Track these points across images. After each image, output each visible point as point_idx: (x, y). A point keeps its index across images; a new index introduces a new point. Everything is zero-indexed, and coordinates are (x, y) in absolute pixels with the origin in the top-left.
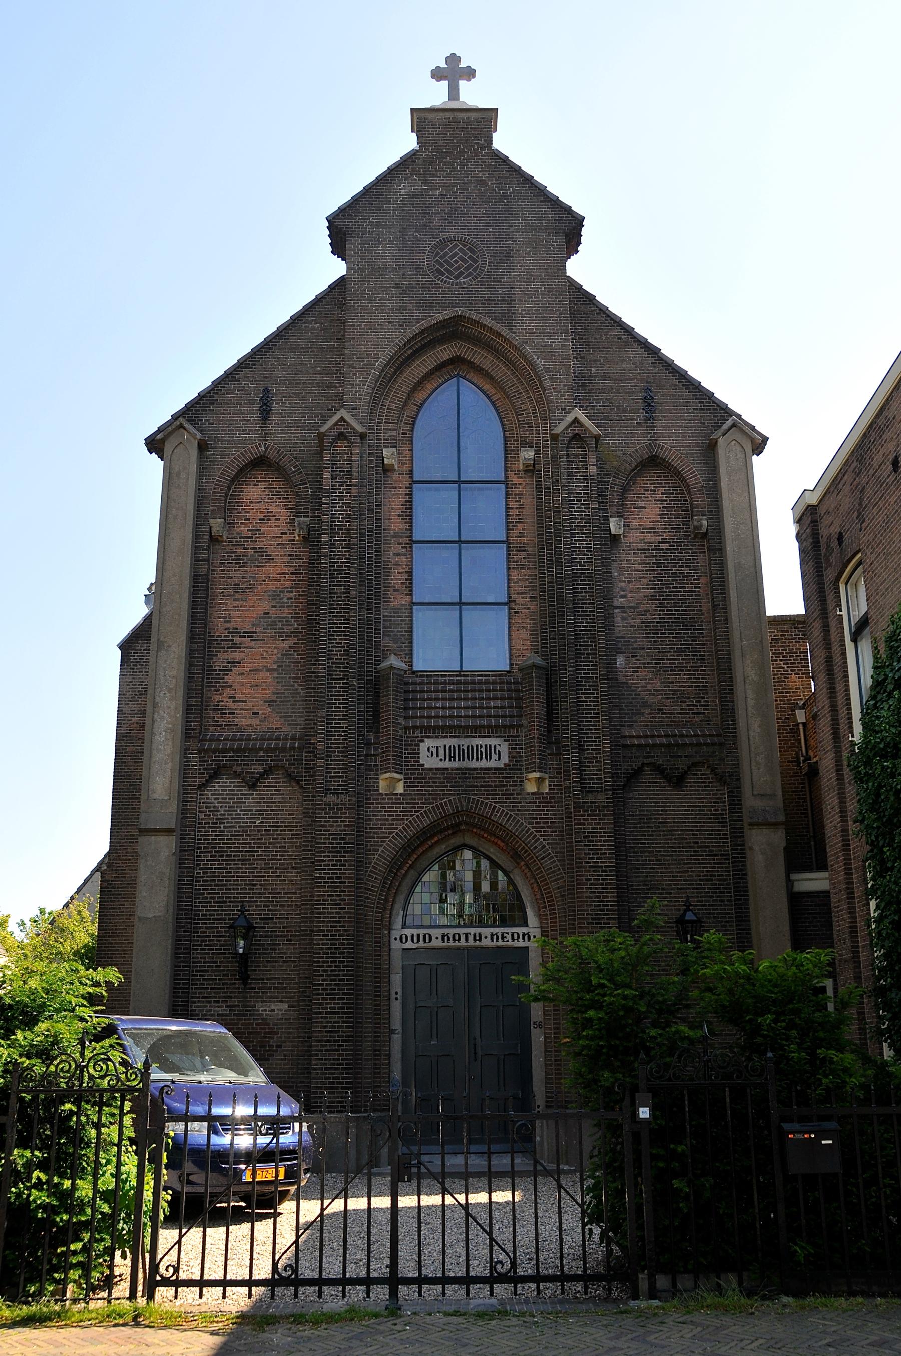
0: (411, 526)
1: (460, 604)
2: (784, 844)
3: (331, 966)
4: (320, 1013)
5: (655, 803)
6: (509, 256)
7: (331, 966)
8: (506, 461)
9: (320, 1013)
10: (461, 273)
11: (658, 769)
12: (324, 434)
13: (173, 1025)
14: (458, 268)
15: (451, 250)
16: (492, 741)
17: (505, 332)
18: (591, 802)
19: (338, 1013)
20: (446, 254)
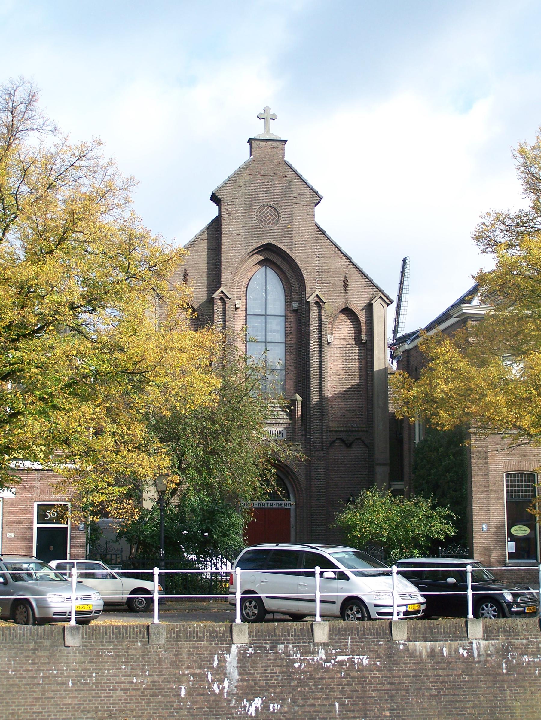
6: (291, 214)
10: (270, 222)
11: (342, 440)
14: (269, 219)
15: (266, 210)
17: (288, 251)
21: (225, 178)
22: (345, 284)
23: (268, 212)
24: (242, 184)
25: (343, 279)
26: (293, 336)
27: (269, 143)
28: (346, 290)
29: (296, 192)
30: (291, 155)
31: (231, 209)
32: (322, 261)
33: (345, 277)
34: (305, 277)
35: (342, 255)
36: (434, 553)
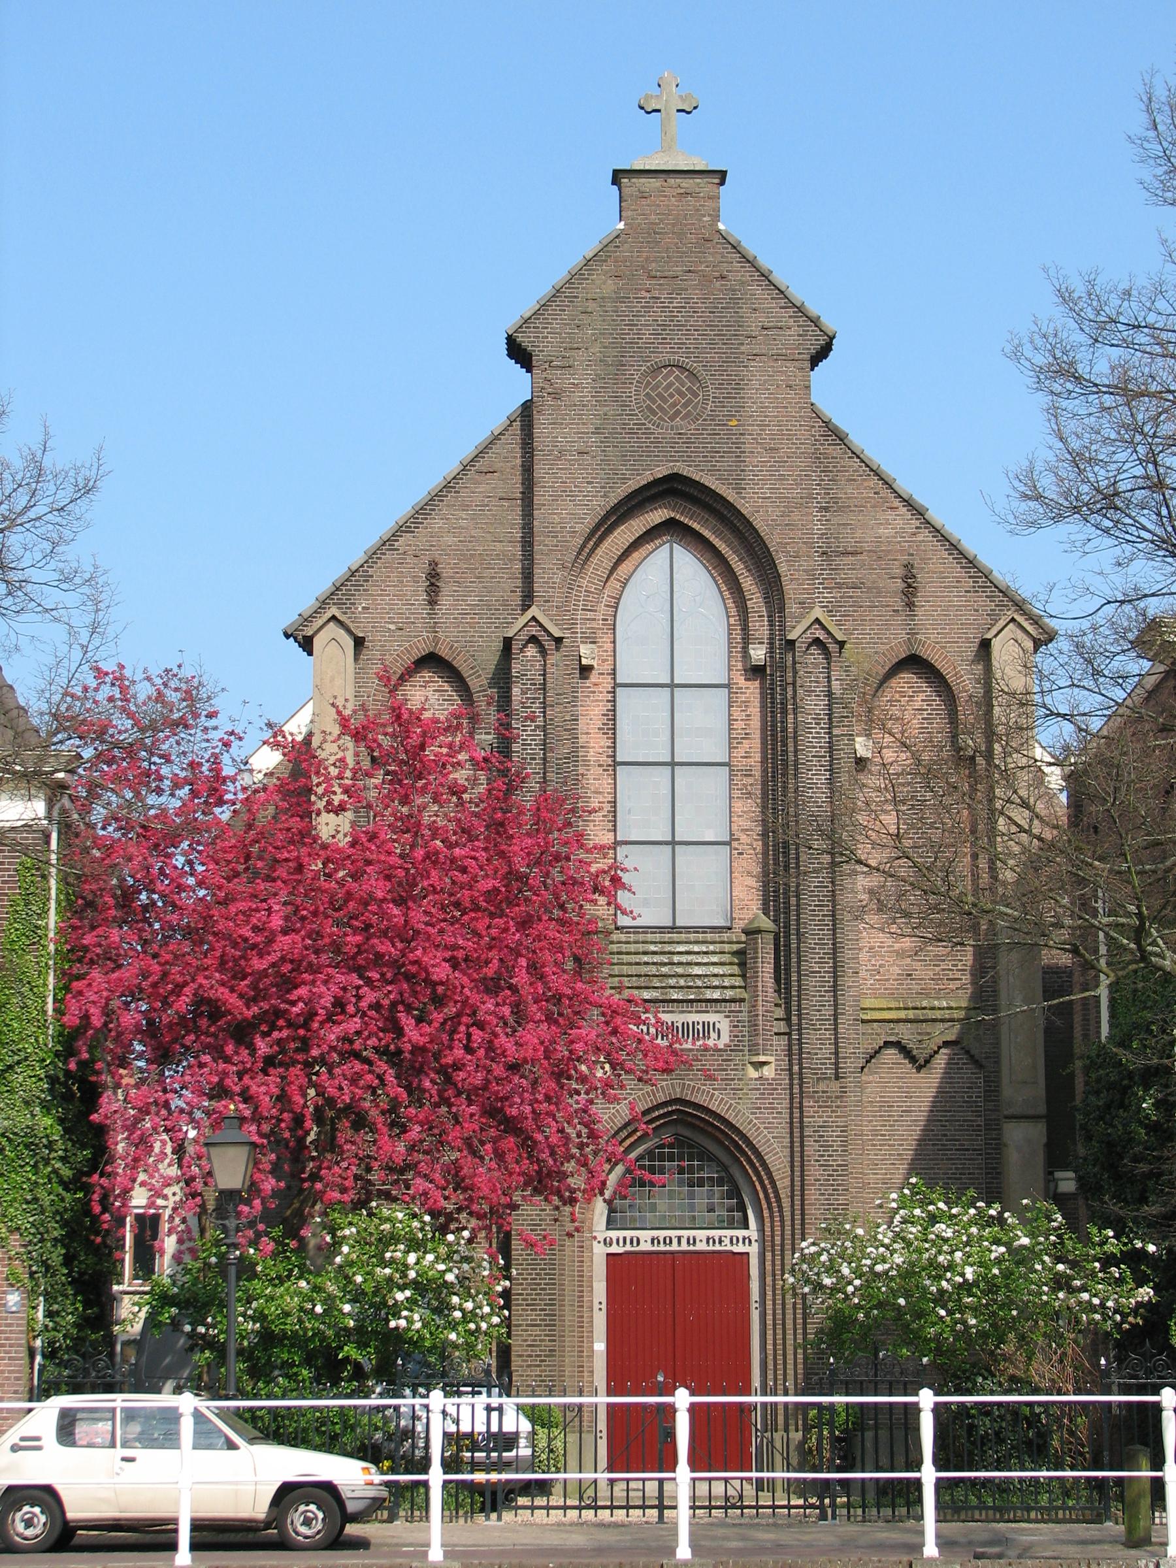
0: (614, 743)
1: (673, 843)
2: (1044, 1140)
3: (531, 1274)
4: (520, 1325)
5: (899, 1087)
6: (739, 387)
7: (531, 1274)
8: (729, 657)
9: (520, 1325)
10: (678, 413)
11: (899, 1046)
12: (510, 639)
13: (917, 1429)
14: (674, 405)
16: (711, 1018)
18: (823, 1092)
19: (540, 1325)
20: (657, 386)
21: (544, 290)
22: (910, 586)
23: (671, 385)
24: (591, 306)
25: (899, 571)
26: (753, 746)
27: (671, 181)
28: (910, 605)
29: (753, 322)
30: (738, 216)
31: (562, 380)
32: (835, 521)
33: (908, 566)
34: (783, 568)
35: (896, 503)
36: (529, 1482)
